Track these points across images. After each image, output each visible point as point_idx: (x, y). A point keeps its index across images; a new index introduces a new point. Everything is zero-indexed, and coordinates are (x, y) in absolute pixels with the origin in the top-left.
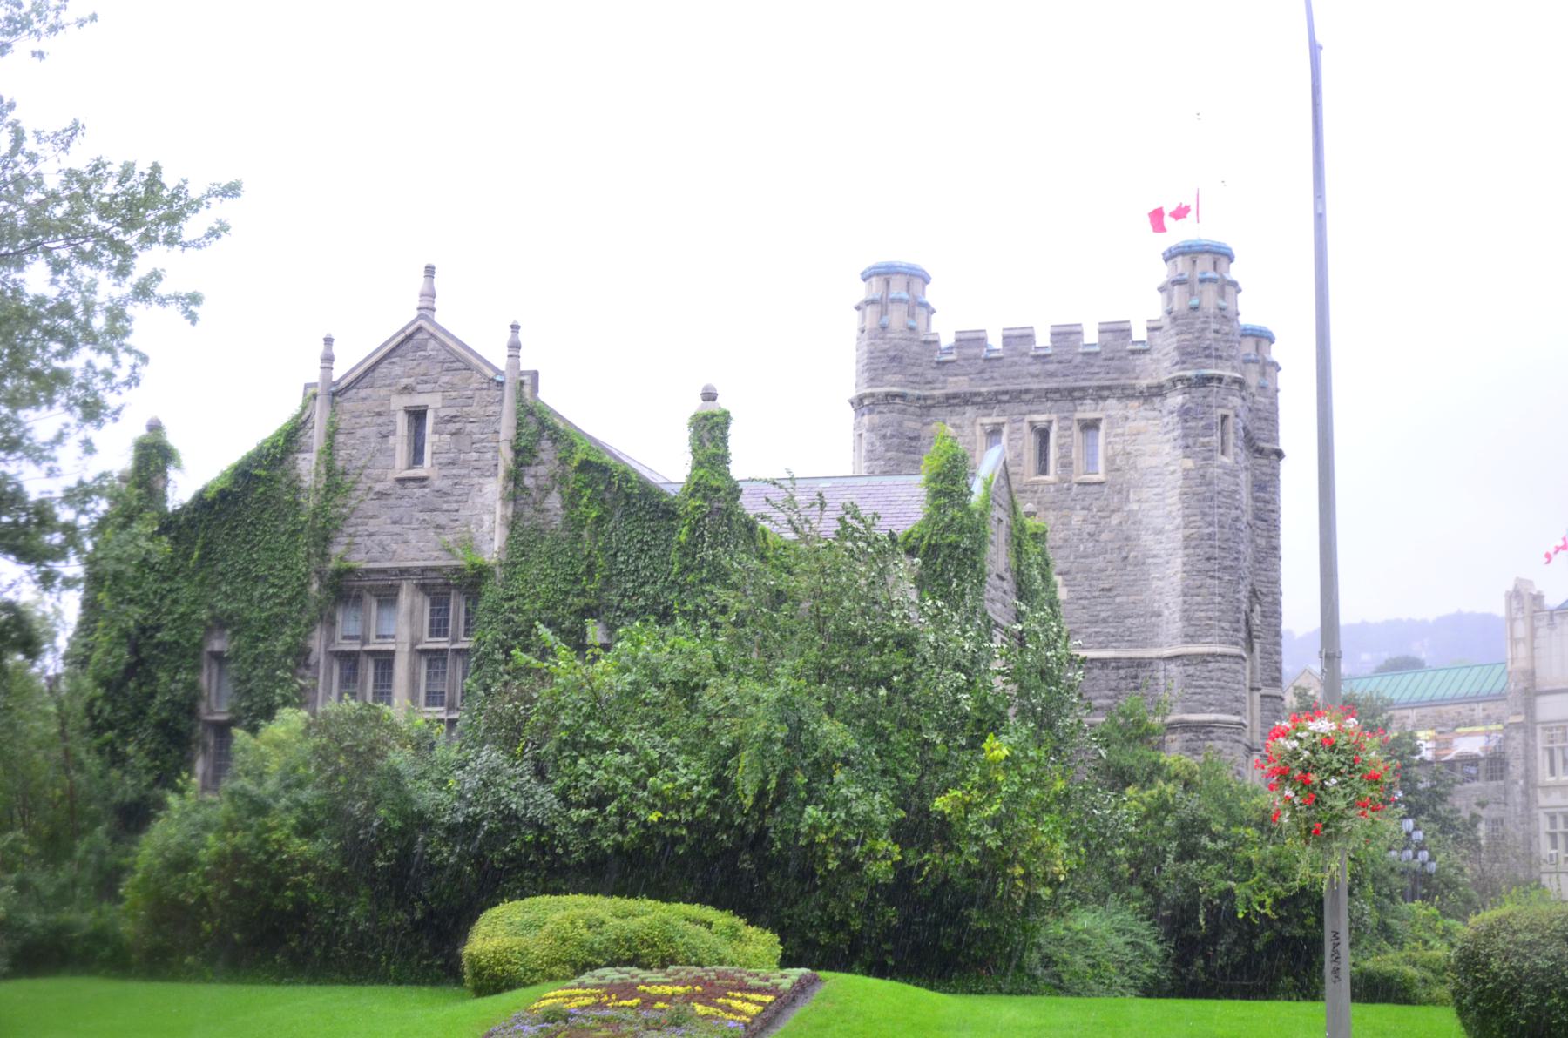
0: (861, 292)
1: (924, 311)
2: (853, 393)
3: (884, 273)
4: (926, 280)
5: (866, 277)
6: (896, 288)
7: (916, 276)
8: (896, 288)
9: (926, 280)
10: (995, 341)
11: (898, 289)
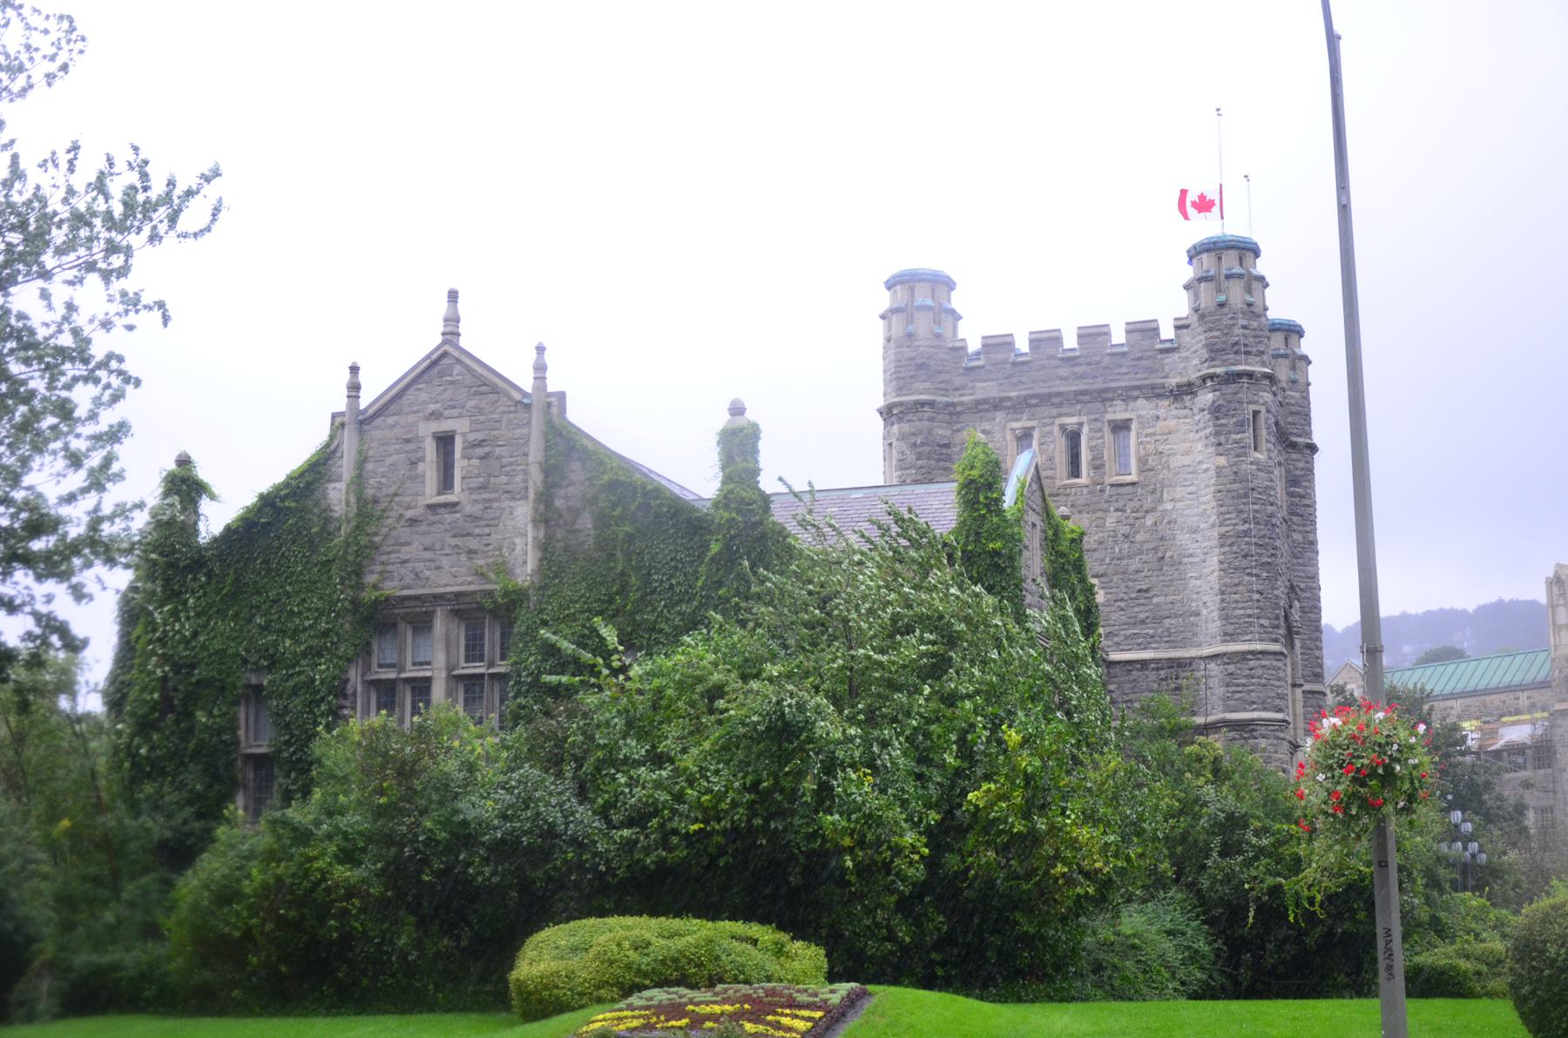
0: (884, 301)
1: (950, 318)
2: (880, 402)
3: (902, 282)
4: (950, 285)
5: (890, 285)
6: (919, 299)
7: (942, 283)
8: (919, 299)
9: (950, 285)
10: (1023, 345)
11: (923, 297)
